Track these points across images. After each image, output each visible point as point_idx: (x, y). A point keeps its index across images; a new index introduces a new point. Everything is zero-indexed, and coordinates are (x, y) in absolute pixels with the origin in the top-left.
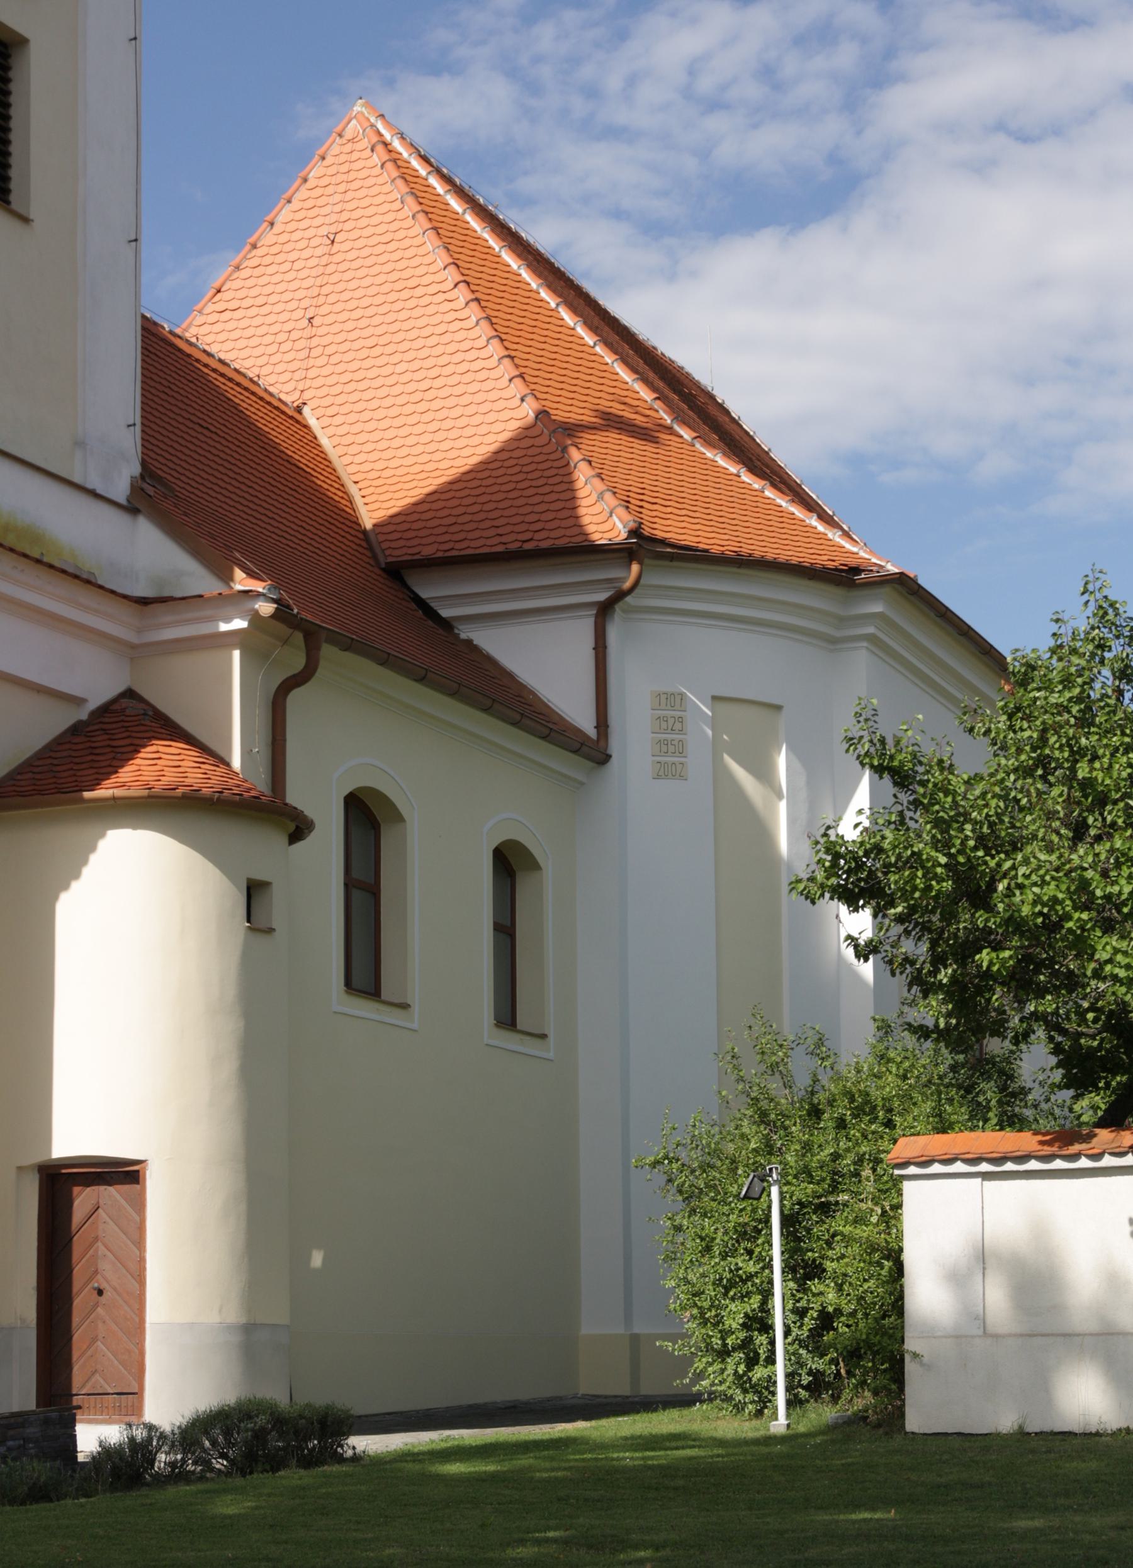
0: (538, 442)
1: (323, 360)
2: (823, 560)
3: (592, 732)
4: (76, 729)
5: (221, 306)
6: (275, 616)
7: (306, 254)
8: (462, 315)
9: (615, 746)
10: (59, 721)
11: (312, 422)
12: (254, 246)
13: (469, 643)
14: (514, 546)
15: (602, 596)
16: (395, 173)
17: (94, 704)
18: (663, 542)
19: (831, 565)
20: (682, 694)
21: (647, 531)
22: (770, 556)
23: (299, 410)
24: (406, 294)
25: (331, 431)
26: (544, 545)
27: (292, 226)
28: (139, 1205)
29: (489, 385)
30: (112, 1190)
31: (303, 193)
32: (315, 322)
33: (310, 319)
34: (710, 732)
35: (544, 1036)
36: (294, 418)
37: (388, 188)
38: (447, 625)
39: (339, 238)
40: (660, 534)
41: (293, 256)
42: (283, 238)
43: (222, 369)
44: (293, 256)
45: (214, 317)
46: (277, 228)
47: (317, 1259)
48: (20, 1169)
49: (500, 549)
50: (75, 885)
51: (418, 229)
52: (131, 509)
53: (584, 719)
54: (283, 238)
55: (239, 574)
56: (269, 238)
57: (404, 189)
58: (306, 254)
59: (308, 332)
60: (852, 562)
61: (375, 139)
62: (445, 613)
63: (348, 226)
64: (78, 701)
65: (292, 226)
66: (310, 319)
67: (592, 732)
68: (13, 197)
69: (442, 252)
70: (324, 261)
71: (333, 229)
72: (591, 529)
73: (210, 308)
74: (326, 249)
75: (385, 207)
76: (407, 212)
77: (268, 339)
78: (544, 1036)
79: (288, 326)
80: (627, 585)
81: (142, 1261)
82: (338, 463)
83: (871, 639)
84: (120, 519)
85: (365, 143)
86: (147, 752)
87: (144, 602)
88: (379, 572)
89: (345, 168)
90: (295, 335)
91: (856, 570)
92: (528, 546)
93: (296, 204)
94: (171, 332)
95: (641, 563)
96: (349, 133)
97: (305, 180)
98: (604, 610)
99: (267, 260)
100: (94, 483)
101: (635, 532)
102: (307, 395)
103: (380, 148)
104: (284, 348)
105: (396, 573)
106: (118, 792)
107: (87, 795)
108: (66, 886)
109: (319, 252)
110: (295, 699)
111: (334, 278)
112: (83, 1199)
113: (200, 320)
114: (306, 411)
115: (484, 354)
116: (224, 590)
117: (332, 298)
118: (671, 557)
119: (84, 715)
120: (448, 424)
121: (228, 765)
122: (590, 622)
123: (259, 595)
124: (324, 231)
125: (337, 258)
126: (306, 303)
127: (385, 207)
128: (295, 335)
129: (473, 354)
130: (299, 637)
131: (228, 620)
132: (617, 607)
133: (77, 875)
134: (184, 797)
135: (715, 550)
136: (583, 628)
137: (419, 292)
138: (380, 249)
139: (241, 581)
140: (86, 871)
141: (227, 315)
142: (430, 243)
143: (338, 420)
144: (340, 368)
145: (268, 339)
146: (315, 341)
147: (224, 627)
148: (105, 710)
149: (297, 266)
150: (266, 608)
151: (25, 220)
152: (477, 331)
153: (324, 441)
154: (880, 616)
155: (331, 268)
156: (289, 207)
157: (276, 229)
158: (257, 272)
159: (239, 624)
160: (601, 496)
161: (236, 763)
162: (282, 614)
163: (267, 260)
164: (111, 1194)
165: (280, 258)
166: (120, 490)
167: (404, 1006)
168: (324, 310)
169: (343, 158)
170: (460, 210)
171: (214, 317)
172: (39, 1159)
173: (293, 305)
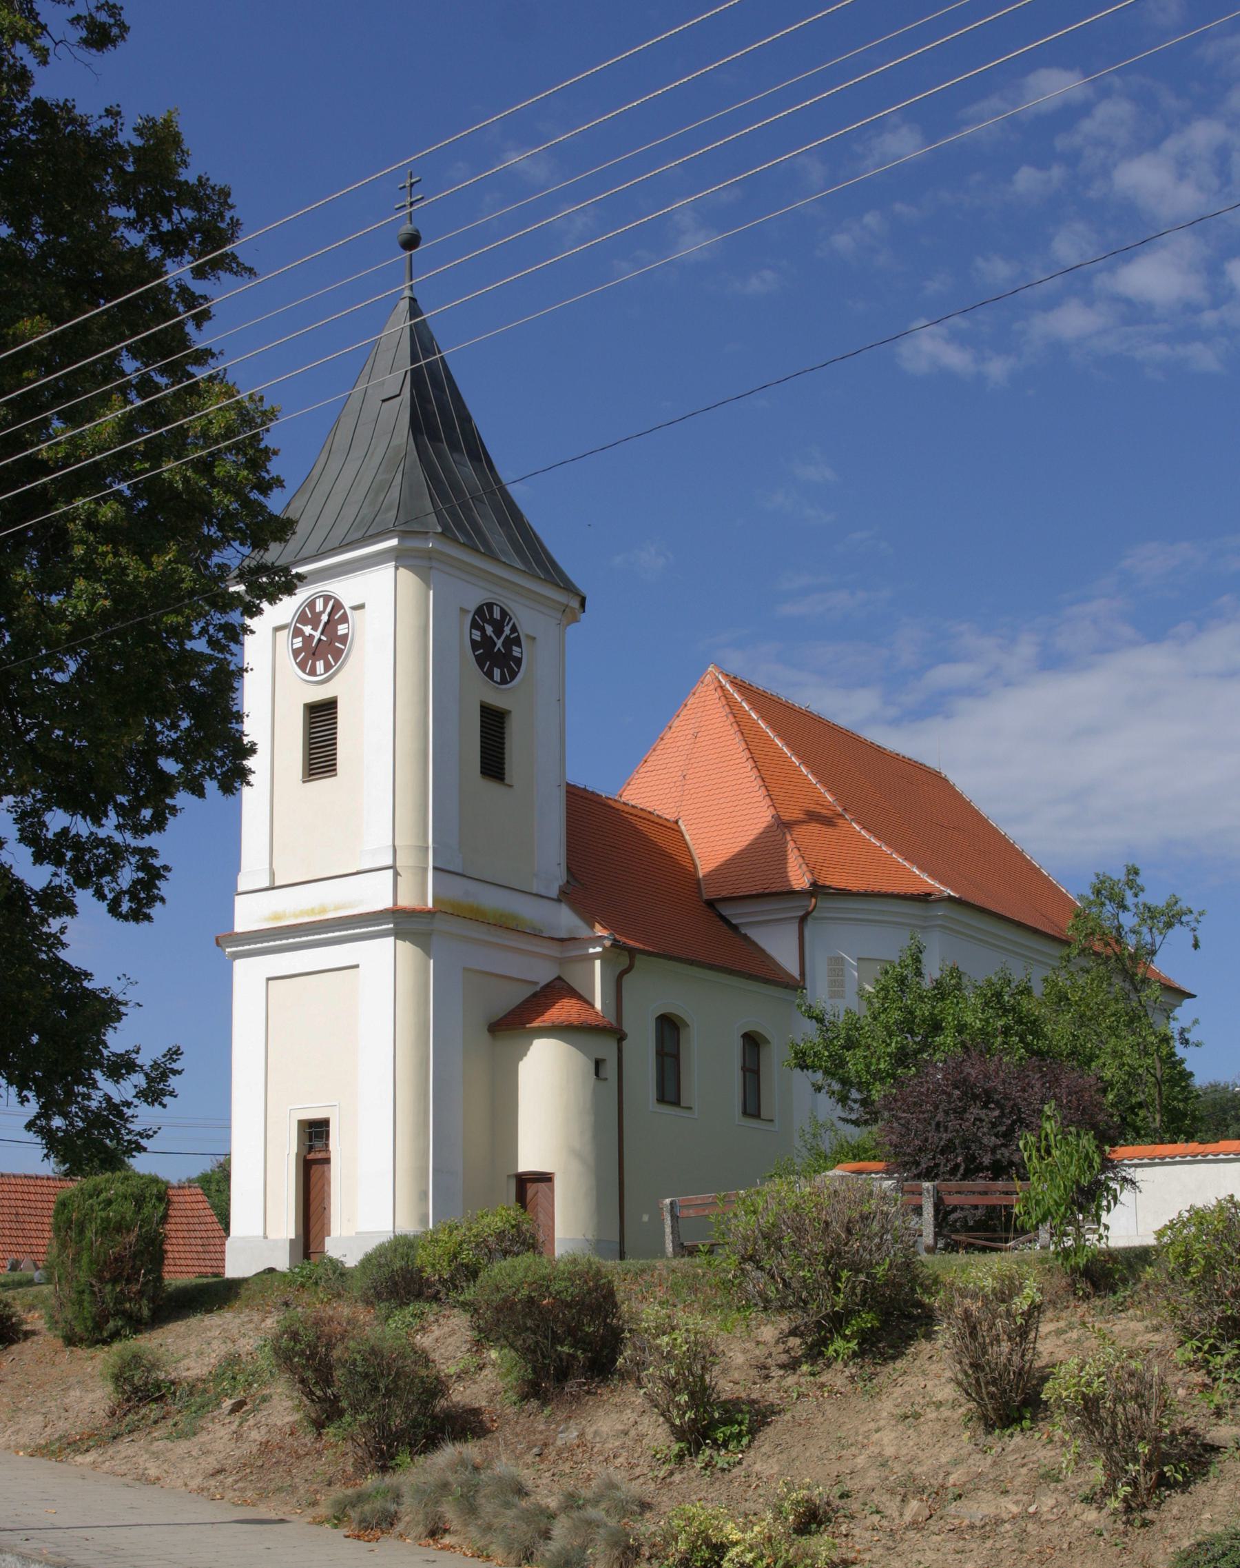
0: (777, 838)
2: (912, 890)
3: (798, 977)
4: (535, 995)
5: (645, 770)
6: (612, 945)
7: (685, 743)
8: (748, 775)
10: (528, 992)
11: (683, 828)
14: (760, 891)
15: (801, 913)
17: (542, 983)
18: (829, 887)
19: (917, 892)
20: (843, 958)
21: (820, 883)
22: (883, 891)
23: (676, 822)
25: (690, 832)
26: (774, 890)
27: (680, 728)
28: (552, 1191)
30: (543, 1184)
32: (687, 777)
33: (684, 776)
34: (856, 974)
36: (672, 828)
37: (721, 710)
38: (735, 928)
40: (828, 883)
41: (679, 744)
44: (679, 744)
45: (643, 775)
47: (646, 1218)
49: (754, 893)
50: (525, 1059)
51: (732, 731)
52: (559, 900)
53: (793, 969)
54: (675, 735)
55: (598, 927)
57: (728, 711)
58: (685, 743)
59: (683, 783)
60: (928, 890)
61: (717, 685)
62: (734, 922)
64: (536, 983)
65: (680, 728)
66: (684, 776)
67: (798, 977)
68: (507, 776)
69: (743, 743)
70: (692, 746)
71: (696, 730)
72: (793, 883)
74: (693, 741)
75: (720, 719)
76: (728, 722)
78: (772, 1121)
79: (674, 780)
80: (810, 909)
81: (553, 1213)
84: (555, 904)
85: (712, 687)
86: (558, 1006)
87: (562, 940)
89: (703, 699)
90: (678, 784)
91: (930, 895)
92: (767, 891)
93: (681, 718)
94: (607, 798)
95: (816, 898)
97: (686, 705)
98: (803, 920)
100: (543, 892)
101: (814, 884)
102: (681, 814)
103: (719, 689)
104: (673, 790)
105: (711, 904)
106: (541, 1024)
107: (528, 1026)
108: (522, 1059)
109: (689, 742)
110: (626, 978)
111: (696, 755)
112: (531, 1189)
113: (637, 776)
114: (680, 822)
116: (591, 935)
117: (695, 765)
119: (538, 988)
120: (740, 829)
121: (593, 1006)
122: (797, 925)
123: (605, 937)
124: (691, 732)
125: (697, 745)
126: (682, 768)
127: (720, 719)
128: (678, 784)
129: (753, 794)
130: (626, 953)
131: (594, 948)
132: (809, 918)
133: (526, 1055)
134: (567, 1026)
135: (855, 889)
136: (794, 928)
138: (717, 740)
139: (600, 931)
145: (666, 786)
146: (686, 787)
147: (591, 951)
148: (547, 986)
149: (680, 749)
150: (608, 943)
151: (511, 786)
152: (755, 783)
153: (687, 837)
155: (694, 750)
156: (679, 719)
157: (672, 730)
158: (663, 752)
159: (599, 949)
161: (598, 1005)
162: (615, 944)
164: (542, 1186)
165: (673, 745)
166: (554, 893)
167: (690, 1108)
168: (690, 772)
169: (703, 694)
170: (755, 717)
172: (514, 1172)
173: (677, 769)
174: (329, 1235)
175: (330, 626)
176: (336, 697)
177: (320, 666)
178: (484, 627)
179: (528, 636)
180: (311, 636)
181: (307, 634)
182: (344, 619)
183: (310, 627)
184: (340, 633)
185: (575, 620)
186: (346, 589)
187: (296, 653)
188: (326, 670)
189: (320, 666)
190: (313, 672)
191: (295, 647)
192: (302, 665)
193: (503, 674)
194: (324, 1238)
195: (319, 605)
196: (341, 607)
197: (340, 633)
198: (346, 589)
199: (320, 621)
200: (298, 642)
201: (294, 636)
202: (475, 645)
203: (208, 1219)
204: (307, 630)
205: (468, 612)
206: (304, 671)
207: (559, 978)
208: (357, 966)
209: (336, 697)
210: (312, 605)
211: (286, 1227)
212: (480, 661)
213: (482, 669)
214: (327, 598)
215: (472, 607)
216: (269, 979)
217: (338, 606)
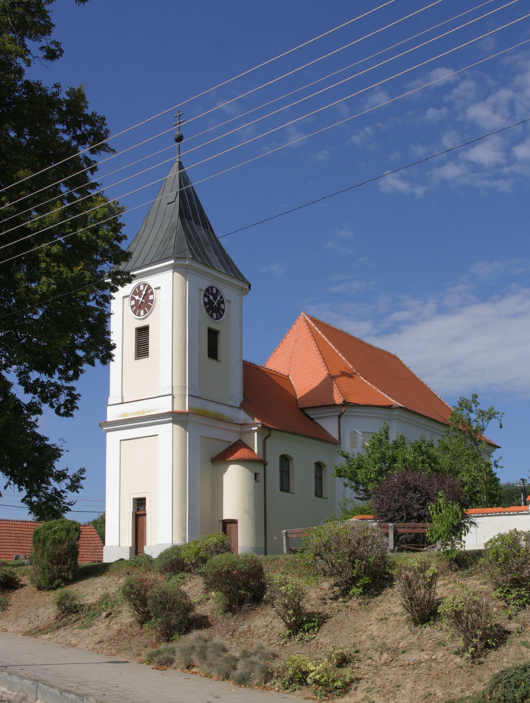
1: (293, 366)
2: (385, 404)
3: (338, 440)
4: (230, 447)
5: (275, 355)
6: (262, 427)
7: (291, 344)
9: (342, 443)
10: (227, 446)
11: (291, 378)
12: (282, 342)
13: (316, 422)
14: (322, 404)
15: (339, 413)
16: (308, 327)
17: (233, 442)
18: (351, 403)
19: (386, 405)
20: (356, 432)
23: (288, 376)
24: (308, 352)
25: (294, 380)
26: (328, 404)
28: (237, 527)
29: (322, 371)
30: (233, 524)
31: (291, 331)
32: (292, 358)
33: (291, 358)
34: (362, 438)
35: (327, 498)
36: (286, 379)
37: (306, 330)
38: (312, 419)
39: (297, 341)
40: (350, 401)
41: (289, 344)
42: (287, 341)
43: (271, 372)
44: (289, 344)
45: (274, 357)
46: (287, 338)
48: (219, 521)
49: (320, 405)
50: (226, 473)
52: (240, 408)
53: (336, 437)
54: (287, 341)
55: (256, 419)
56: (285, 340)
57: (309, 331)
58: (291, 344)
60: (391, 404)
62: (312, 417)
63: (299, 338)
64: (230, 442)
66: (291, 358)
67: (338, 440)
68: (219, 357)
69: (315, 344)
72: (336, 401)
73: (274, 355)
74: (295, 343)
77: (284, 361)
78: (327, 498)
79: (287, 359)
80: (343, 412)
82: (294, 387)
83: (396, 419)
85: (303, 321)
86: (239, 451)
87: (241, 424)
88: (298, 410)
89: (299, 326)
91: (392, 406)
92: (325, 404)
94: (259, 366)
96: (300, 319)
98: (340, 416)
99: (285, 345)
101: (344, 402)
102: (290, 373)
103: (305, 322)
105: (302, 410)
106: (233, 459)
108: (225, 473)
110: (268, 441)
112: (229, 526)
113: (272, 357)
114: (290, 376)
115: (321, 365)
118: (352, 406)
119: (231, 444)
121: (254, 451)
123: (259, 423)
124: (294, 339)
125: (296, 345)
127: (306, 334)
128: (289, 360)
130: (268, 430)
133: (226, 471)
134: (243, 460)
135: (361, 404)
136: (336, 419)
137: (311, 352)
139: (256, 421)
140: (228, 471)
141: (277, 356)
142: (313, 342)
143: (295, 378)
144: (296, 367)
145: (284, 361)
146: (292, 362)
147: (253, 429)
148: (235, 443)
150: (260, 426)
151: (220, 361)
153: (292, 382)
154: (398, 414)
155: (295, 347)
156: (289, 334)
159: (256, 428)
160: (339, 394)
161: (256, 451)
163: (285, 345)
164: (233, 525)
165: (287, 345)
166: (238, 405)
167: (293, 493)
168: (294, 356)
171: (274, 357)
174: (146, 545)
175: (146, 296)
176: (149, 325)
177: (142, 312)
178: (209, 296)
179: (227, 300)
180: (138, 300)
181: (137, 299)
182: (152, 293)
183: (138, 296)
184: (150, 299)
185: (246, 293)
186: (153, 281)
187: (132, 307)
188: (145, 314)
189: (142, 312)
190: (139, 315)
191: (132, 304)
192: (135, 312)
193: (217, 316)
194: (143, 547)
195: (142, 288)
196: (151, 288)
197: (150, 299)
198: (153, 281)
199: (142, 294)
200: (133, 303)
201: (132, 300)
202: (205, 304)
203: (96, 539)
204: (137, 298)
205: (203, 290)
206: (135, 314)
207: (240, 440)
208: (157, 435)
209: (149, 325)
210: (139, 287)
211: (128, 542)
212: (208, 310)
213: (208, 313)
214: (145, 285)
215: (204, 288)
216: (121, 440)
217: (149, 288)
